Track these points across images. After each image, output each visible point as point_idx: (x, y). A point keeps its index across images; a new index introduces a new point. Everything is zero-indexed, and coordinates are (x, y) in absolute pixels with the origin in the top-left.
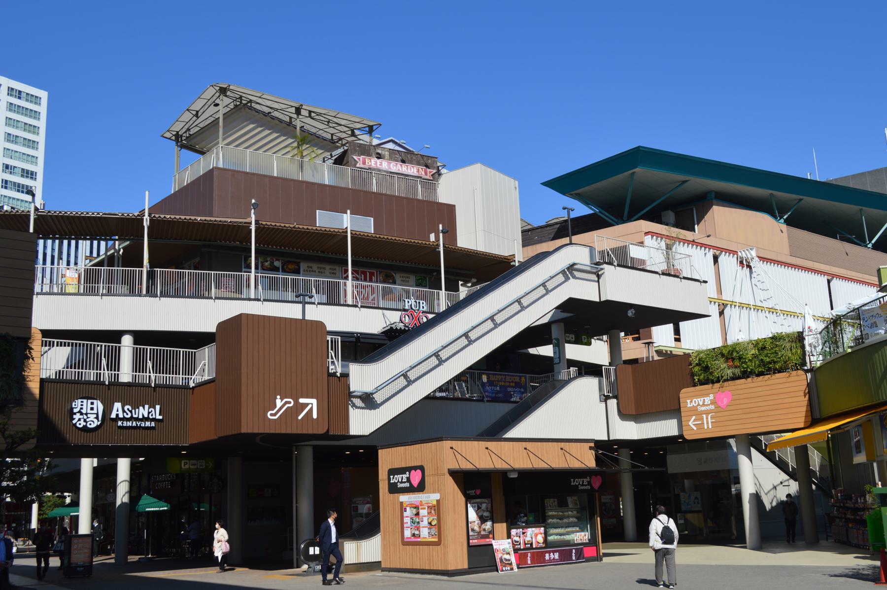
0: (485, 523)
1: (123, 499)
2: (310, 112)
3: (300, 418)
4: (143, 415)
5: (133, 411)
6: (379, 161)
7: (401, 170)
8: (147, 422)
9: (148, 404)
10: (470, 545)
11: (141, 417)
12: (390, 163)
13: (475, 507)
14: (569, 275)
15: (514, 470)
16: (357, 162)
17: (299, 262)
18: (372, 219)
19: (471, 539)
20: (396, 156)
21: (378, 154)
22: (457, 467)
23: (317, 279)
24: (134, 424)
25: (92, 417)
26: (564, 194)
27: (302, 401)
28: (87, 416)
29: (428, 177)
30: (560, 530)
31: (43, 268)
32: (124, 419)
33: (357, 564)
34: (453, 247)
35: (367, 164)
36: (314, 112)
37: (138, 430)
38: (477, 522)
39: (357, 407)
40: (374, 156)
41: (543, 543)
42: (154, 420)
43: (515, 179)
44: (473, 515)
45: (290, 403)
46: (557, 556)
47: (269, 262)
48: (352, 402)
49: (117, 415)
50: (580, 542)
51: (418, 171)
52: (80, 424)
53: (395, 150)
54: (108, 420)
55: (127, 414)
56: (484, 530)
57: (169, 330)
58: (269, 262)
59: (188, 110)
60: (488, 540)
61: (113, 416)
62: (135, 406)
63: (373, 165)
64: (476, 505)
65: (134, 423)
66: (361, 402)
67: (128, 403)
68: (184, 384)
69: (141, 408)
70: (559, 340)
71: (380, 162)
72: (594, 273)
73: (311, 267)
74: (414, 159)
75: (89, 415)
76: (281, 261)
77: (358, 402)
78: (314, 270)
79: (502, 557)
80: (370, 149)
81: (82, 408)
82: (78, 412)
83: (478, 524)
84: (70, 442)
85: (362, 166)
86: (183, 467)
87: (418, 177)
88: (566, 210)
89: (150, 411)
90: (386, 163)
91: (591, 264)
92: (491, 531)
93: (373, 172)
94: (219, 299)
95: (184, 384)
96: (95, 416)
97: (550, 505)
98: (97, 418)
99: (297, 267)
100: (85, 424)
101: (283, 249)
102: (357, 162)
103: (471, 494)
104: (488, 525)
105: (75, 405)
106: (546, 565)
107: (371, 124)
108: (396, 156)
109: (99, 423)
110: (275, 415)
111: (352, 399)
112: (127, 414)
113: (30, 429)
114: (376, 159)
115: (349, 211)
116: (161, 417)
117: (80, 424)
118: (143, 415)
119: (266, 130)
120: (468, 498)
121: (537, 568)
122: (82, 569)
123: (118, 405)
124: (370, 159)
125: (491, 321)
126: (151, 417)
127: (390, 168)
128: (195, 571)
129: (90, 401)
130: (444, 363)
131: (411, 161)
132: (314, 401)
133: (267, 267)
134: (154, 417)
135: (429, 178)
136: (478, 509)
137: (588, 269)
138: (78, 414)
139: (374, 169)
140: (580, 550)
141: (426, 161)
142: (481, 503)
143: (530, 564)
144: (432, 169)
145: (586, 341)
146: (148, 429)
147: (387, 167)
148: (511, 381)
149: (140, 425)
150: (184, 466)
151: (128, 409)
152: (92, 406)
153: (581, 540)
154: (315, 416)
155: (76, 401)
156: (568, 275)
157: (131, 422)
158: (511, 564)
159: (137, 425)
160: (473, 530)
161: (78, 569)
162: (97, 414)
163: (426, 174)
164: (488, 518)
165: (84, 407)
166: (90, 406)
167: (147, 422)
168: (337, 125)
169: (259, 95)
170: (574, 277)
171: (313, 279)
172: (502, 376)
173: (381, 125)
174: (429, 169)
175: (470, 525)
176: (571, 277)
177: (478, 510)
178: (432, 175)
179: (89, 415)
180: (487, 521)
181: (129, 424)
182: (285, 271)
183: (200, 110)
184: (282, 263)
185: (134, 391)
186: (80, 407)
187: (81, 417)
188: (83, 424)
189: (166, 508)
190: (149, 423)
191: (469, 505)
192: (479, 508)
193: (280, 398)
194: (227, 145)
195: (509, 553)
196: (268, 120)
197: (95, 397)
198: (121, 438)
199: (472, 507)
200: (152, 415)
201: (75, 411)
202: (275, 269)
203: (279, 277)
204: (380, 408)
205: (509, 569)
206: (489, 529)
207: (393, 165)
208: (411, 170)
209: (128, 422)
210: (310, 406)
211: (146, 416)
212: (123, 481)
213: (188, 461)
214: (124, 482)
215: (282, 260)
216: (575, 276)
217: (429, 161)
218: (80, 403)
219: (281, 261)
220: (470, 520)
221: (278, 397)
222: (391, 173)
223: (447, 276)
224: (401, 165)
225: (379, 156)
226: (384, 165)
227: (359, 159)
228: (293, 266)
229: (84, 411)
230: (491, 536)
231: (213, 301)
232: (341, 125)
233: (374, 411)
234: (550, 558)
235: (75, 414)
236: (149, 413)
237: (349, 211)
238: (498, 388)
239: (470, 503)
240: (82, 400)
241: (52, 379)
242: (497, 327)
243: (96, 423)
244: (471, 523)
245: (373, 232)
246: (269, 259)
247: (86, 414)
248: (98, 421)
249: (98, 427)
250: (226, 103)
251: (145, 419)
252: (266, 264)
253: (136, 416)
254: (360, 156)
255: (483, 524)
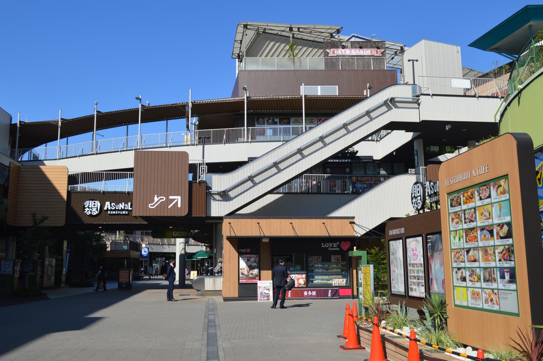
0: (252, 270)
1: (182, 252)
2: (299, 28)
3: (169, 207)
4: (121, 208)
5: (116, 206)
6: (343, 50)
7: (359, 53)
8: (123, 212)
9: (124, 202)
10: (240, 283)
11: (120, 209)
12: (352, 50)
13: (245, 260)
14: (392, 106)
15: (265, 237)
16: (329, 53)
17: (290, 118)
18: (337, 86)
19: (241, 279)
20: (356, 45)
21: (343, 46)
22: (328, 235)
23: (311, 126)
24: (117, 213)
25: (94, 209)
26: (485, 50)
27: (171, 197)
28: (92, 209)
29: (378, 55)
30: (319, 277)
31: (166, 134)
32: (111, 210)
33: (214, 291)
34: (362, 97)
35: (335, 53)
36: (301, 28)
37: (120, 216)
38: (246, 269)
39: (216, 200)
40: (340, 48)
41: (304, 284)
42: (127, 210)
43: (457, 45)
44: (243, 264)
45: (163, 199)
46: (314, 293)
47: (271, 120)
48: (213, 197)
49: (108, 208)
50: (342, 285)
51: (371, 52)
52: (88, 213)
53: (355, 42)
54: (104, 211)
55: (113, 208)
56: (252, 274)
57: (227, 161)
58: (271, 120)
59: (235, 41)
60: (255, 280)
61: (105, 208)
62: (117, 203)
63: (340, 53)
64: (246, 258)
65: (117, 212)
66: (219, 197)
67: (109, 200)
68: (83, 190)
69: (120, 204)
70: (418, 151)
71: (344, 51)
72: (416, 103)
73: (298, 120)
74: (369, 45)
75: (93, 209)
76: (278, 118)
77: (217, 197)
78: (300, 121)
79: (262, 291)
80: (338, 44)
81: (89, 205)
82: (87, 207)
83: (247, 270)
84: (84, 222)
85: (332, 55)
86: (174, 235)
87: (371, 56)
88: (411, 62)
89: (125, 205)
90: (349, 51)
91: (413, 97)
92: (258, 275)
93: (340, 58)
94: (262, 142)
95: (83, 190)
96: (96, 209)
97: (314, 260)
98: (97, 210)
99: (288, 121)
100: (91, 213)
101: (336, 111)
102: (329, 53)
103: (242, 252)
104: (256, 271)
105: (86, 204)
106: (304, 299)
107: (338, 28)
108: (356, 45)
109: (98, 212)
110: (153, 206)
111: (213, 195)
112: (113, 208)
113: (43, 216)
114: (342, 49)
115: (303, 84)
116: (131, 209)
117: (88, 213)
118: (121, 208)
119: (271, 43)
120: (240, 254)
121: (296, 300)
122: (125, 286)
123: (108, 203)
124: (338, 50)
125: (321, 142)
126: (125, 209)
127: (352, 53)
128: (185, 290)
129: (93, 202)
130: (282, 171)
131: (366, 47)
132: (179, 198)
133: (270, 123)
134: (127, 208)
135: (379, 55)
136: (247, 261)
137: (411, 100)
138: (87, 208)
139: (340, 56)
140: (335, 291)
141: (377, 46)
142: (250, 258)
143: (290, 297)
144: (381, 49)
145: (449, 150)
146: (124, 215)
147: (349, 53)
148: (376, 180)
149: (120, 213)
150: (175, 235)
151: (113, 205)
152: (94, 204)
153: (339, 284)
154: (179, 206)
155: (86, 201)
156: (391, 106)
157: (115, 212)
158: (269, 296)
159: (118, 213)
160: (242, 274)
161: (123, 285)
162: (97, 208)
163: (377, 53)
164: (256, 267)
165: (91, 205)
166: (93, 204)
167: (123, 212)
168: (321, 33)
169: (266, 25)
170: (397, 107)
171: (300, 126)
172: (369, 178)
173: (342, 28)
174: (379, 49)
175: (240, 270)
176: (393, 108)
177: (247, 261)
178: (381, 53)
179: (93, 209)
180: (254, 268)
181: (114, 212)
182: (280, 124)
183: (242, 38)
184: (279, 120)
185: (117, 195)
186: (88, 204)
187: (89, 209)
188: (90, 213)
189: (207, 257)
190: (125, 212)
191: (240, 258)
192: (248, 260)
193: (157, 197)
194: (272, 57)
195: (269, 290)
196: (279, 38)
197: (96, 199)
198: (111, 220)
199: (243, 259)
200: (126, 208)
201: (86, 206)
202: (276, 123)
203: (255, 128)
204: (233, 200)
205: (266, 299)
206: (255, 273)
207: (354, 51)
208: (366, 52)
209: (113, 212)
210: (176, 200)
211: (123, 208)
212: (181, 243)
213: (177, 232)
214: (182, 243)
215: (279, 118)
216: (398, 106)
217: (380, 44)
218: (88, 203)
219: (278, 118)
220: (240, 268)
221: (156, 196)
222: (352, 56)
223: (306, 119)
224: (359, 50)
225: (344, 47)
226: (348, 52)
227: (330, 51)
228: (286, 121)
229: (90, 207)
230: (257, 278)
231: (250, 143)
232: (323, 33)
233: (229, 202)
234: (308, 294)
235: (86, 208)
236: (125, 207)
237: (303, 84)
238: (365, 185)
239: (241, 257)
240: (95, 201)
241: (98, 191)
242: (326, 146)
243: (97, 212)
244: (241, 270)
245: (338, 95)
246: (271, 118)
247: (92, 208)
248: (98, 211)
249: (97, 215)
250: (251, 34)
251: (122, 210)
252: (270, 121)
253: (118, 208)
254: (331, 49)
255: (251, 270)
